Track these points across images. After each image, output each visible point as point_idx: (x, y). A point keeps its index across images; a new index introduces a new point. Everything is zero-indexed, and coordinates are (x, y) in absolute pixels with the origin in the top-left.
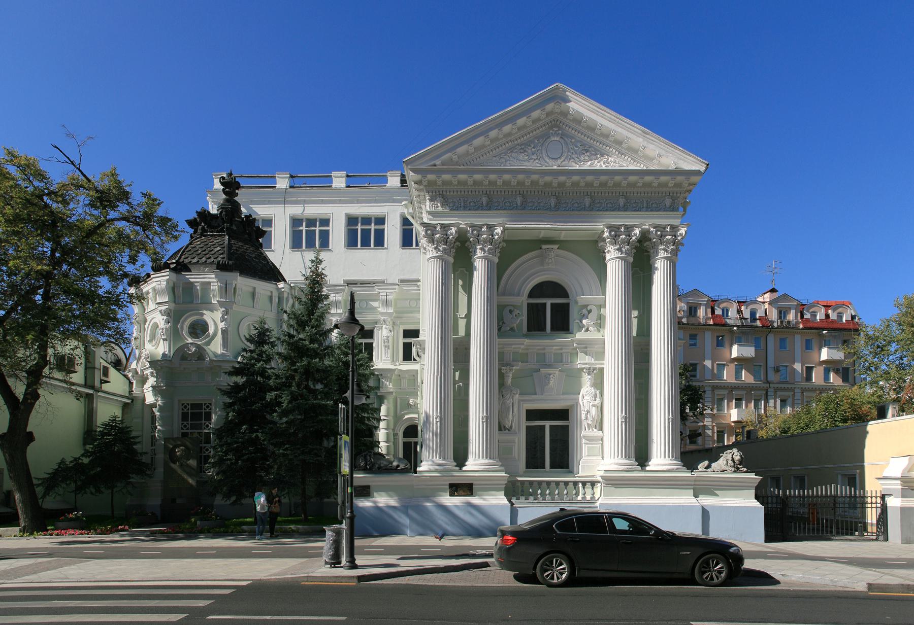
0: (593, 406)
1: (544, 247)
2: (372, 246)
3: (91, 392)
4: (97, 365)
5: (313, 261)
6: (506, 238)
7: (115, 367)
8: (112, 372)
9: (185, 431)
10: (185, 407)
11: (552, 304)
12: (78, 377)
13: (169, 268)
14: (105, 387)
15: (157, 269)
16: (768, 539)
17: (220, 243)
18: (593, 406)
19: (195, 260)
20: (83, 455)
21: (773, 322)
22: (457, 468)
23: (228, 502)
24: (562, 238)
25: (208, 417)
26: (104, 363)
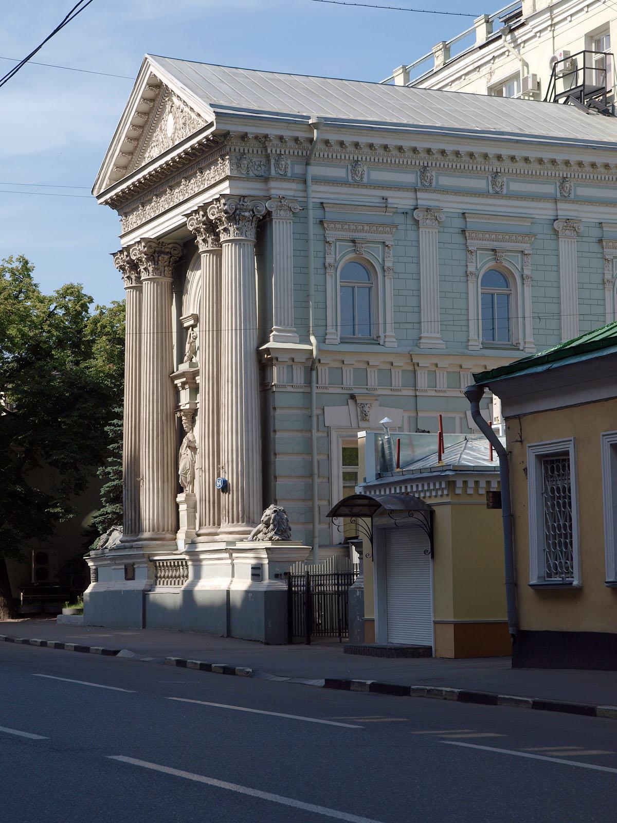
16: (569, 450)
21: (361, 493)
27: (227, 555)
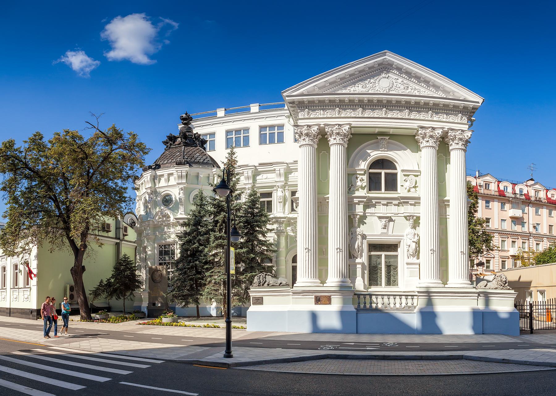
0: (413, 242)
1: (379, 138)
2: (268, 143)
3: (118, 241)
4: (121, 227)
5: (229, 154)
6: (353, 132)
7: (131, 227)
8: (129, 229)
9: (161, 262)
10: (161, 247)
11: (386, 174)
12: (112, 234)
13: (152, 168)
14: (126, 238)
15: (145, 170)
17: (180, 151)
18: (413, 242)
19: (165, 162)
20: (111, 277)
22: (322, 285)
23: (181, 306)
24: (391, 133)
25: (173, 253)
26: (125, 225)
27: (477, 295)
